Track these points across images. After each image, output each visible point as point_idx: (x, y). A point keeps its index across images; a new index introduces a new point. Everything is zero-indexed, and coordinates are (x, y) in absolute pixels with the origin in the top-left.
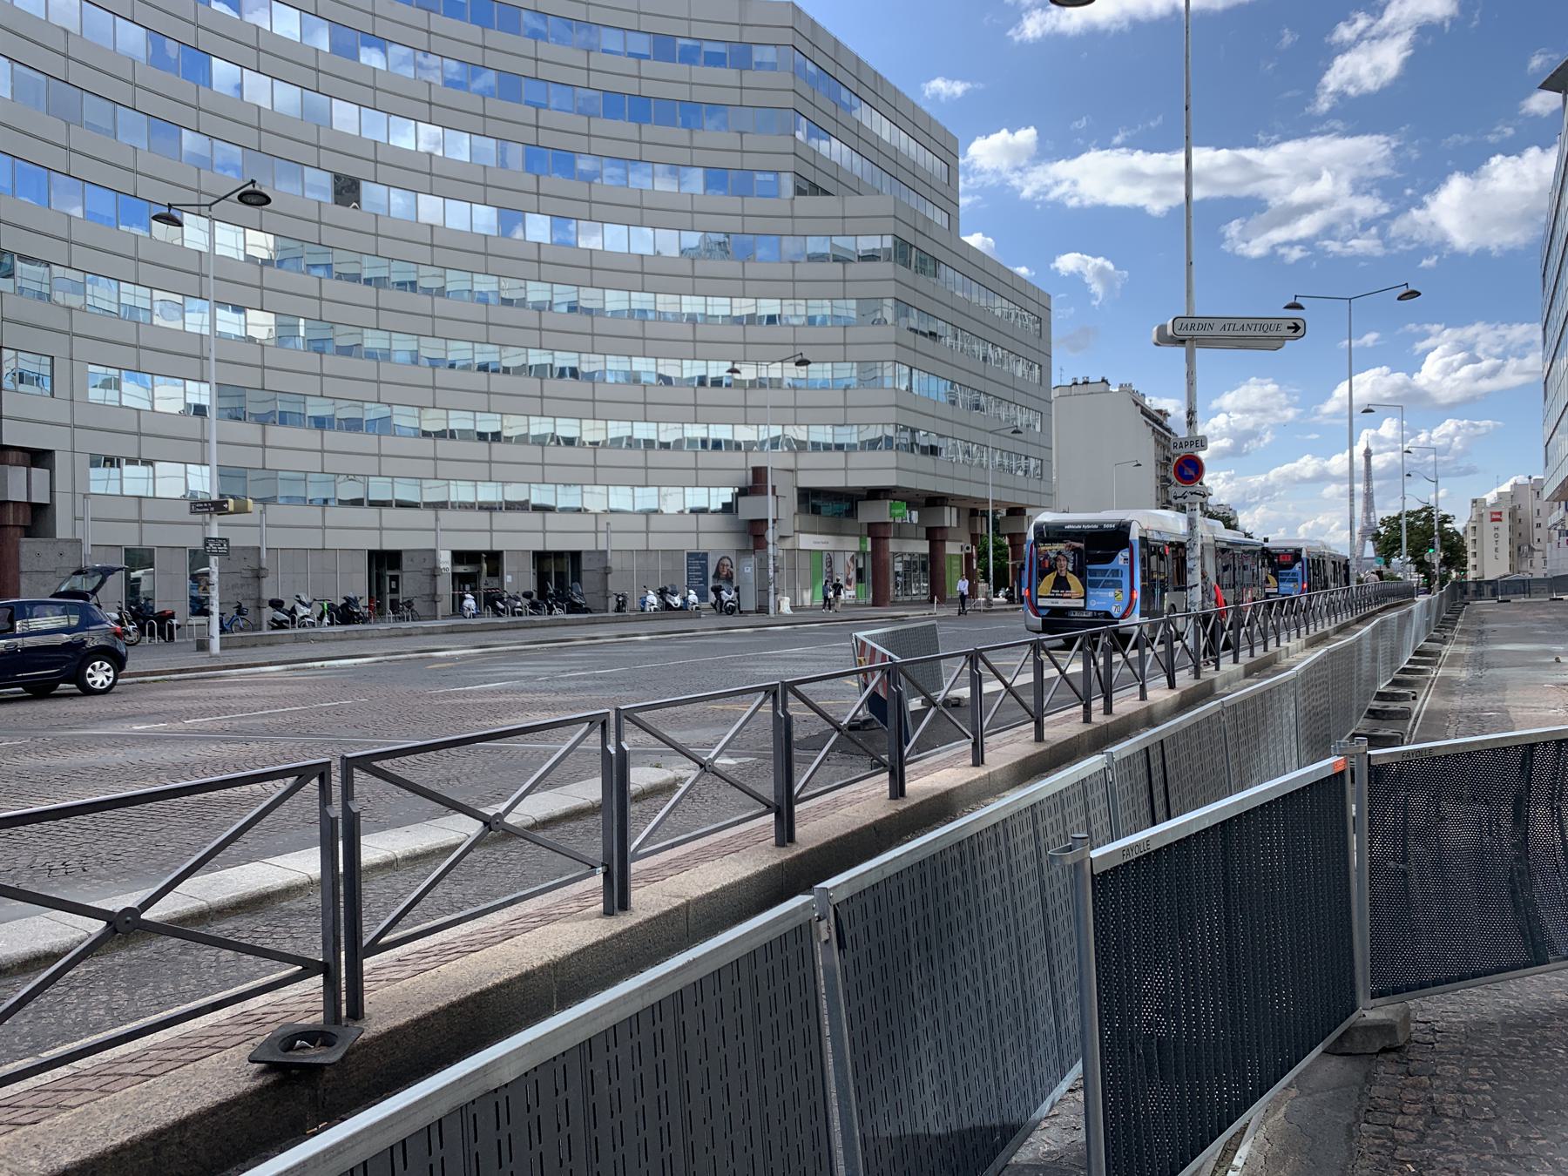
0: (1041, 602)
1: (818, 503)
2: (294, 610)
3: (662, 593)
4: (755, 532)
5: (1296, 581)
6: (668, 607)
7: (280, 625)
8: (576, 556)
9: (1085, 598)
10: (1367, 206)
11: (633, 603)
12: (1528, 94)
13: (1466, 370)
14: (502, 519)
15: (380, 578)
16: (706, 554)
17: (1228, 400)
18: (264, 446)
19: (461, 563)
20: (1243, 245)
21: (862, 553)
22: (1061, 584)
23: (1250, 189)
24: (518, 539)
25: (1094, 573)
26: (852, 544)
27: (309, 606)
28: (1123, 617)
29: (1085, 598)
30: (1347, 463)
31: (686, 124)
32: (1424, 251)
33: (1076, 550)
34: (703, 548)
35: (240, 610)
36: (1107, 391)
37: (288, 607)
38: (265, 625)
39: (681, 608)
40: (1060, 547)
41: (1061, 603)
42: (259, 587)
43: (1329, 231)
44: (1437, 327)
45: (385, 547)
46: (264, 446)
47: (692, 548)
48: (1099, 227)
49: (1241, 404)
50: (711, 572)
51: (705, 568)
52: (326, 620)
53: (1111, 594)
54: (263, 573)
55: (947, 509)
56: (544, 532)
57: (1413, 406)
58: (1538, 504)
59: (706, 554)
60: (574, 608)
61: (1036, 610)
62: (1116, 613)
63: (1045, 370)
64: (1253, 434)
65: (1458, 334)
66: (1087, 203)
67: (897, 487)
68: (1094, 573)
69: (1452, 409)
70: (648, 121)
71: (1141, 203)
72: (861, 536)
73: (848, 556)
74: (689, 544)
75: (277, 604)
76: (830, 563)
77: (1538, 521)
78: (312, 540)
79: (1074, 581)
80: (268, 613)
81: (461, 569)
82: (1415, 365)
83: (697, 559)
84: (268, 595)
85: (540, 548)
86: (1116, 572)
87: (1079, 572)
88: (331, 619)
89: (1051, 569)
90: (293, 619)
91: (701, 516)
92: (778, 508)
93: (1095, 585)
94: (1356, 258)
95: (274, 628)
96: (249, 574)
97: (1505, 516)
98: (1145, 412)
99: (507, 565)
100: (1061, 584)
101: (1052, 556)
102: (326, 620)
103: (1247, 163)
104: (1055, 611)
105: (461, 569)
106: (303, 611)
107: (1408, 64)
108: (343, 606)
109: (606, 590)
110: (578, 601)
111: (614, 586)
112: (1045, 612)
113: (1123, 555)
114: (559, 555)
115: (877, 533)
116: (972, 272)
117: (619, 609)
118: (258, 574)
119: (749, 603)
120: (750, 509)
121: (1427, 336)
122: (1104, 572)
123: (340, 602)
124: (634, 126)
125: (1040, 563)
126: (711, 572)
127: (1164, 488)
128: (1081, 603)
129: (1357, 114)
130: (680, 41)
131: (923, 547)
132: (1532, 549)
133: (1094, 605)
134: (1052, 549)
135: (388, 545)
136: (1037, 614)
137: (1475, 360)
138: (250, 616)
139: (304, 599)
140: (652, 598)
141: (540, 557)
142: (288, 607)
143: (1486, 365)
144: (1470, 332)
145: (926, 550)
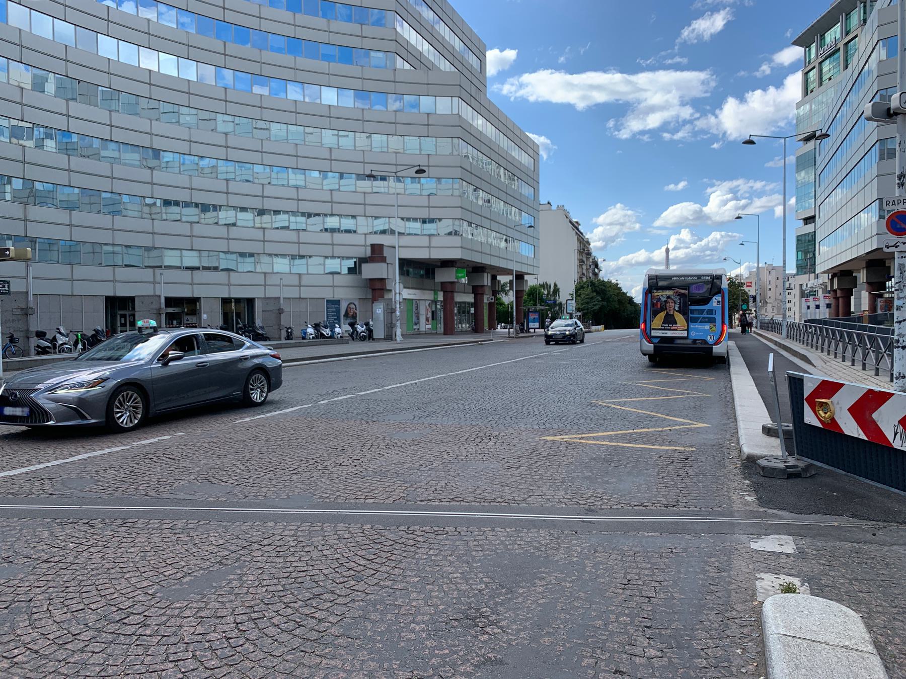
0: (654, 333)
1: (420, 270)
2: (55, 339)
3: (316, 327)
4: (377, 289)
5: (712, 321)
6: (322, 336)
7: (43, 351)
8: (250, 302)
9: (687, 330)
10: (687, 112)
11: (297, 333)
12: (780, 49)
13: (732, 204)
14: (199, 276)
15: (114, 317)
16: (339, 301)
17: (601, 219)
18: (26, 220)
19: (171, 306)
20: (617, 133)
21: (435, 302)
22: (670, 320)
23: (631, 97)
24: (210, 290)
25: (693, 312)
26: (429, 295)
27: (67, 336)
28: (716, 343)
29: (687, 330)
30: (664, 254)
31: (324, 16)
32: (715, 138)
33: (681, 295)
34: (337, 296)
35: (12, 340)
36: (550, 210)
37: (49, 336)
38: (33, 352)
39: (331, 337)
40: (669, 293)
41: (670, 334)
42: (27, 321)
43: (665, 127)
44: (719, 182)
45: (118, 294)
46: (26, 220)
47: (329, 296)
48: (553, 114)
49: (608, 221)
50: (343, 313)
51: (338, 311)
52: (80, 346)
53: (707, 327)
54: (30, 311)
55: (485, 274)
56: (229, 285)
57: (700, 224)
58: (770, 278)
59: (339, 301)
60: (374, 339)
61: (650, 339)
62: (709, 339)
63: (536, 190)
64: (612, 239)
65: (727, 185)
66: (540, 99)
67: (461, 259)
68: (693, 312)
69: (720, 226)
70: (300, 11)
71: (572, 102)
72: (434, 290)
73: (427, 303)
74: (328, 295)
75: (41, 335)
76: (417, 308)
77: (769, 287)
78: (64, 288)
79: (679, 317)
80: (34, 341)
81: (170, 310)
82: (705, 202)
83: (334, 303)
84: (33, 328)
85: (227, 296)
86: (710, 312)
87: (683, 311)
88: (84, 345)
89: (662, 309)
90: (55, 347)
91: (336, 276)
92: (390, 272)
93: (695, 320)
94: (679, 141)
95: (38, 353)
96: (19, 312)
97: (753, 285)
98: (571, 222)
99: (204, 306)
100: (670, 320)
101: (663, 299)
102: (80, 346)
103: (630, 82)
104: (664, 339)
105: (170, 310)
106: (61, 340)
107: (728, 25)
108: (93, 336)
109: (280, 325)
110: (260, 332)
111: (284, 321)
112: (656, 341)
113: (716, 299)
114: (238, 300)
115: (448, 289)
116: (501, 126)
117: (289, 337)
118: (26, 313)
119: (379, 333)
120: (370, 271)
121: (713, 185)
122: (702, 312)
123: (90, 333)
124: (290, 14)
125: (653, 305)
126: (343, 313)
127: (581, 266)
128: (685, 334)
129: (697, 56)
130: (104, 195)
131: (470, 298)
132: (766, 303)
133: (693, 335)
134: (663, 295)
135: (123, 291)
136: (650, 342)
137: (736, 198)
138: (21, 344)
139: (63, 331)
140: (310, 330)
141: (226, 301)
142: (49, 336)
143: (743, 202)
144: (735, 183)
145: (473, 301)
